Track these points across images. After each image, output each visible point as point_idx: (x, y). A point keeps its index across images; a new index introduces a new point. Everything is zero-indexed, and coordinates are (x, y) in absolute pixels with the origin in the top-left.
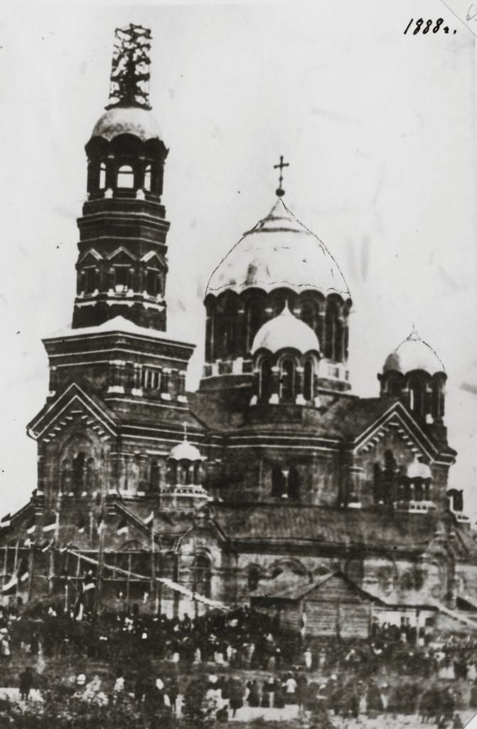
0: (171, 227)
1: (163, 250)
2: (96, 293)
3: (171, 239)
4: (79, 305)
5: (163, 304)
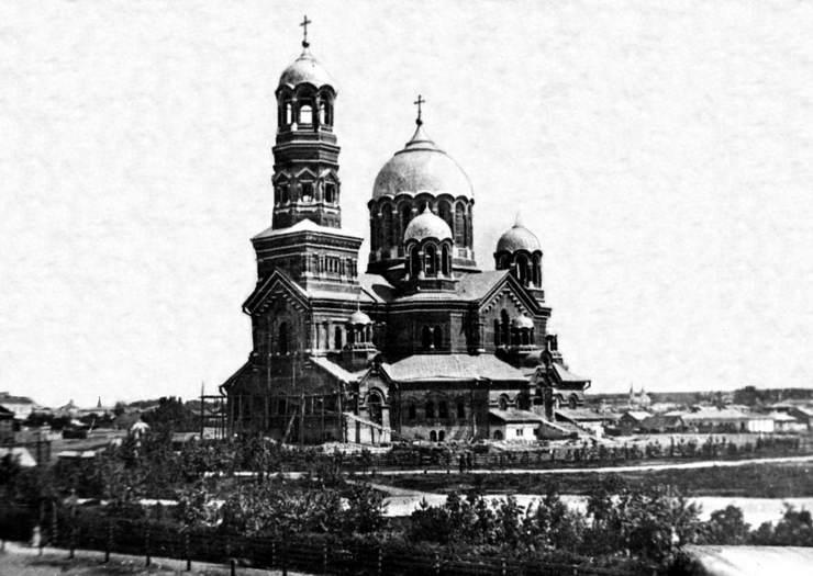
0: (341, 151)
2: (288, 203)
3: (341, 160)
4: (277, 212)
5: (338, 208)
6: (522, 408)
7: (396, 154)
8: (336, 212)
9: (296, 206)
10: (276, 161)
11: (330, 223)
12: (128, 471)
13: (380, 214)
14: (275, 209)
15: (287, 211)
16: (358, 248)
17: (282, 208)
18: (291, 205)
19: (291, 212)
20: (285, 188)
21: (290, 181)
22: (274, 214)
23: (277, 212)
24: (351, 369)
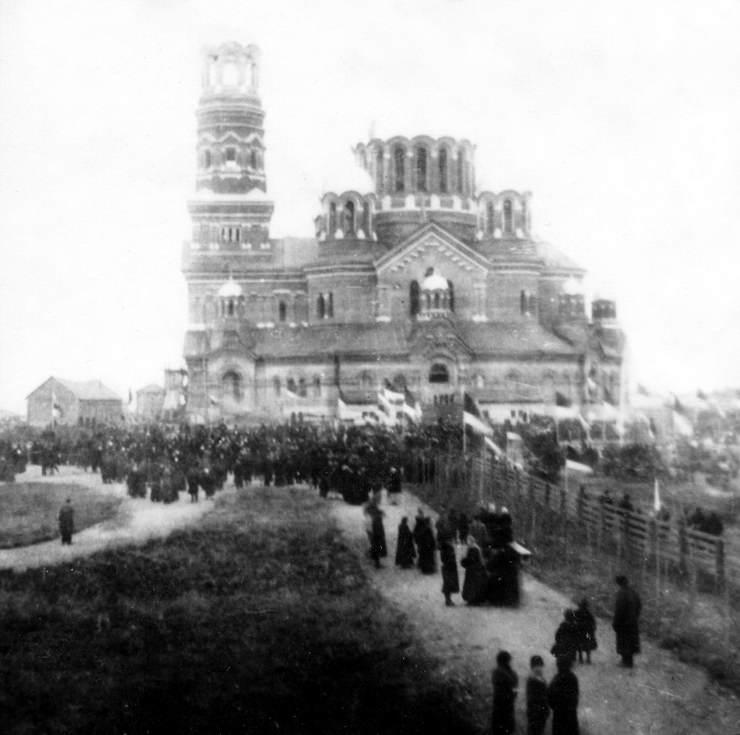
1: (261, 133)
5: (264, 176)
16: (268, 219)
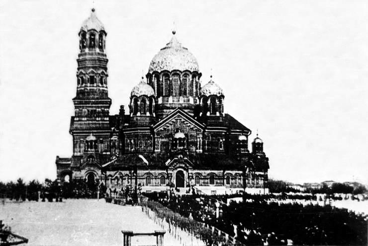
3: (109, 65)
4: (79, 89)
5: (107, 87)
6: (316, 198)
7: (161, 50)
8: (106, 89)
9: (87, 86)
10: (268, 163)
11: (113, 201)
12: (157, 164)
13: (139, 103)
14: (78, 88)
15: (83, 89)
17: (81, 87)
18: (85, 86)
19: (84, 89)
20: (82, 78)
21: (84, 74)
22: (77, 91)
23: (79, 89)
24: (227, 173)
